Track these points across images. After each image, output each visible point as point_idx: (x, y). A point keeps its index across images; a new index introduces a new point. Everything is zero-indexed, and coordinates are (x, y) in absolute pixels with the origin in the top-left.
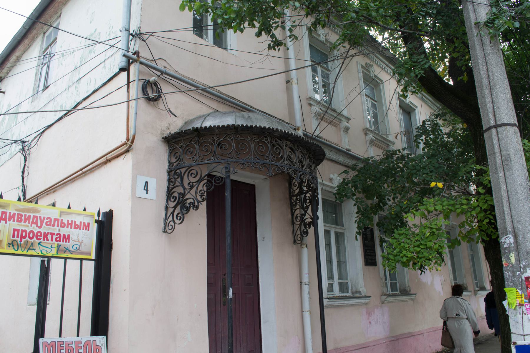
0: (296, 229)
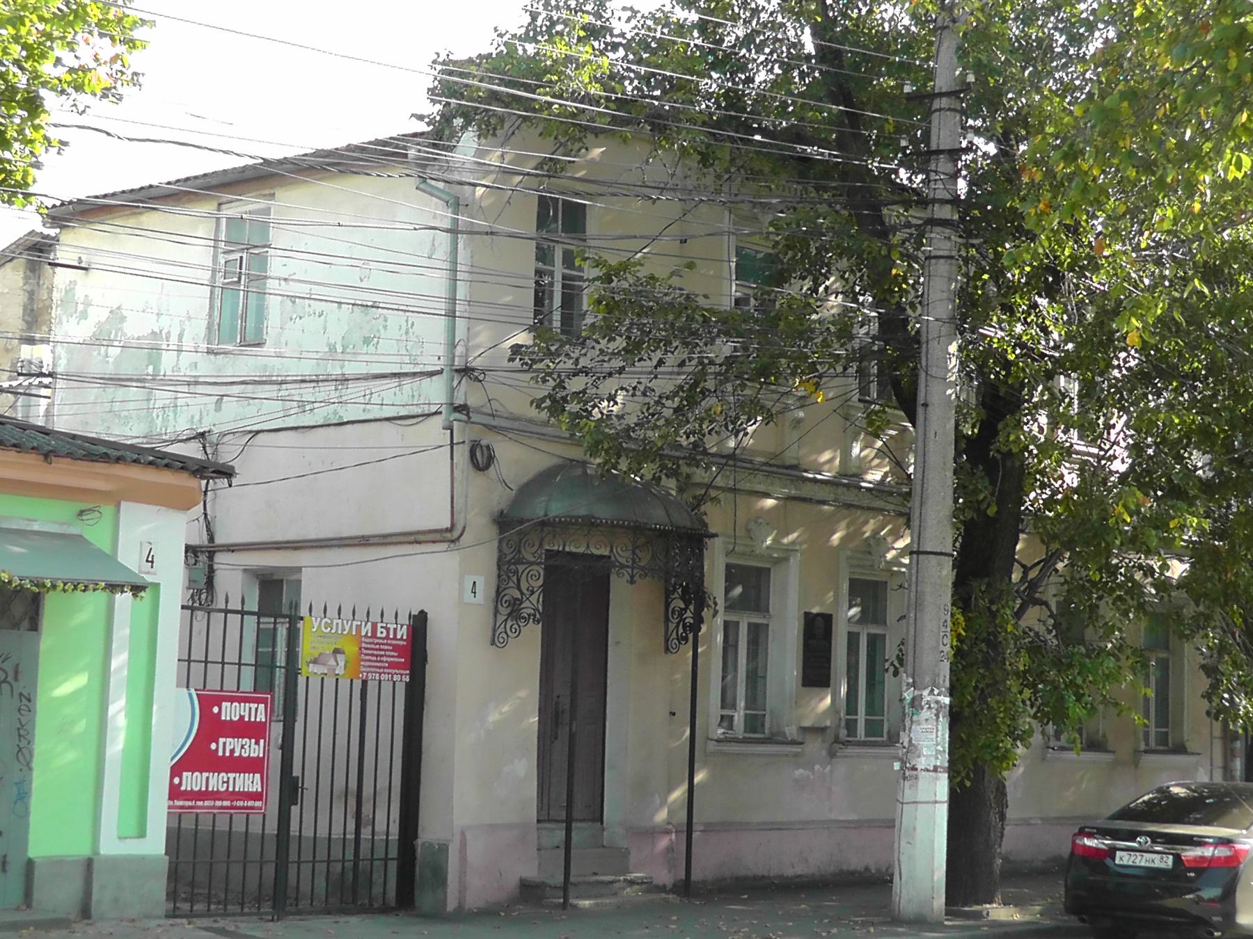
0: (671, 629)
